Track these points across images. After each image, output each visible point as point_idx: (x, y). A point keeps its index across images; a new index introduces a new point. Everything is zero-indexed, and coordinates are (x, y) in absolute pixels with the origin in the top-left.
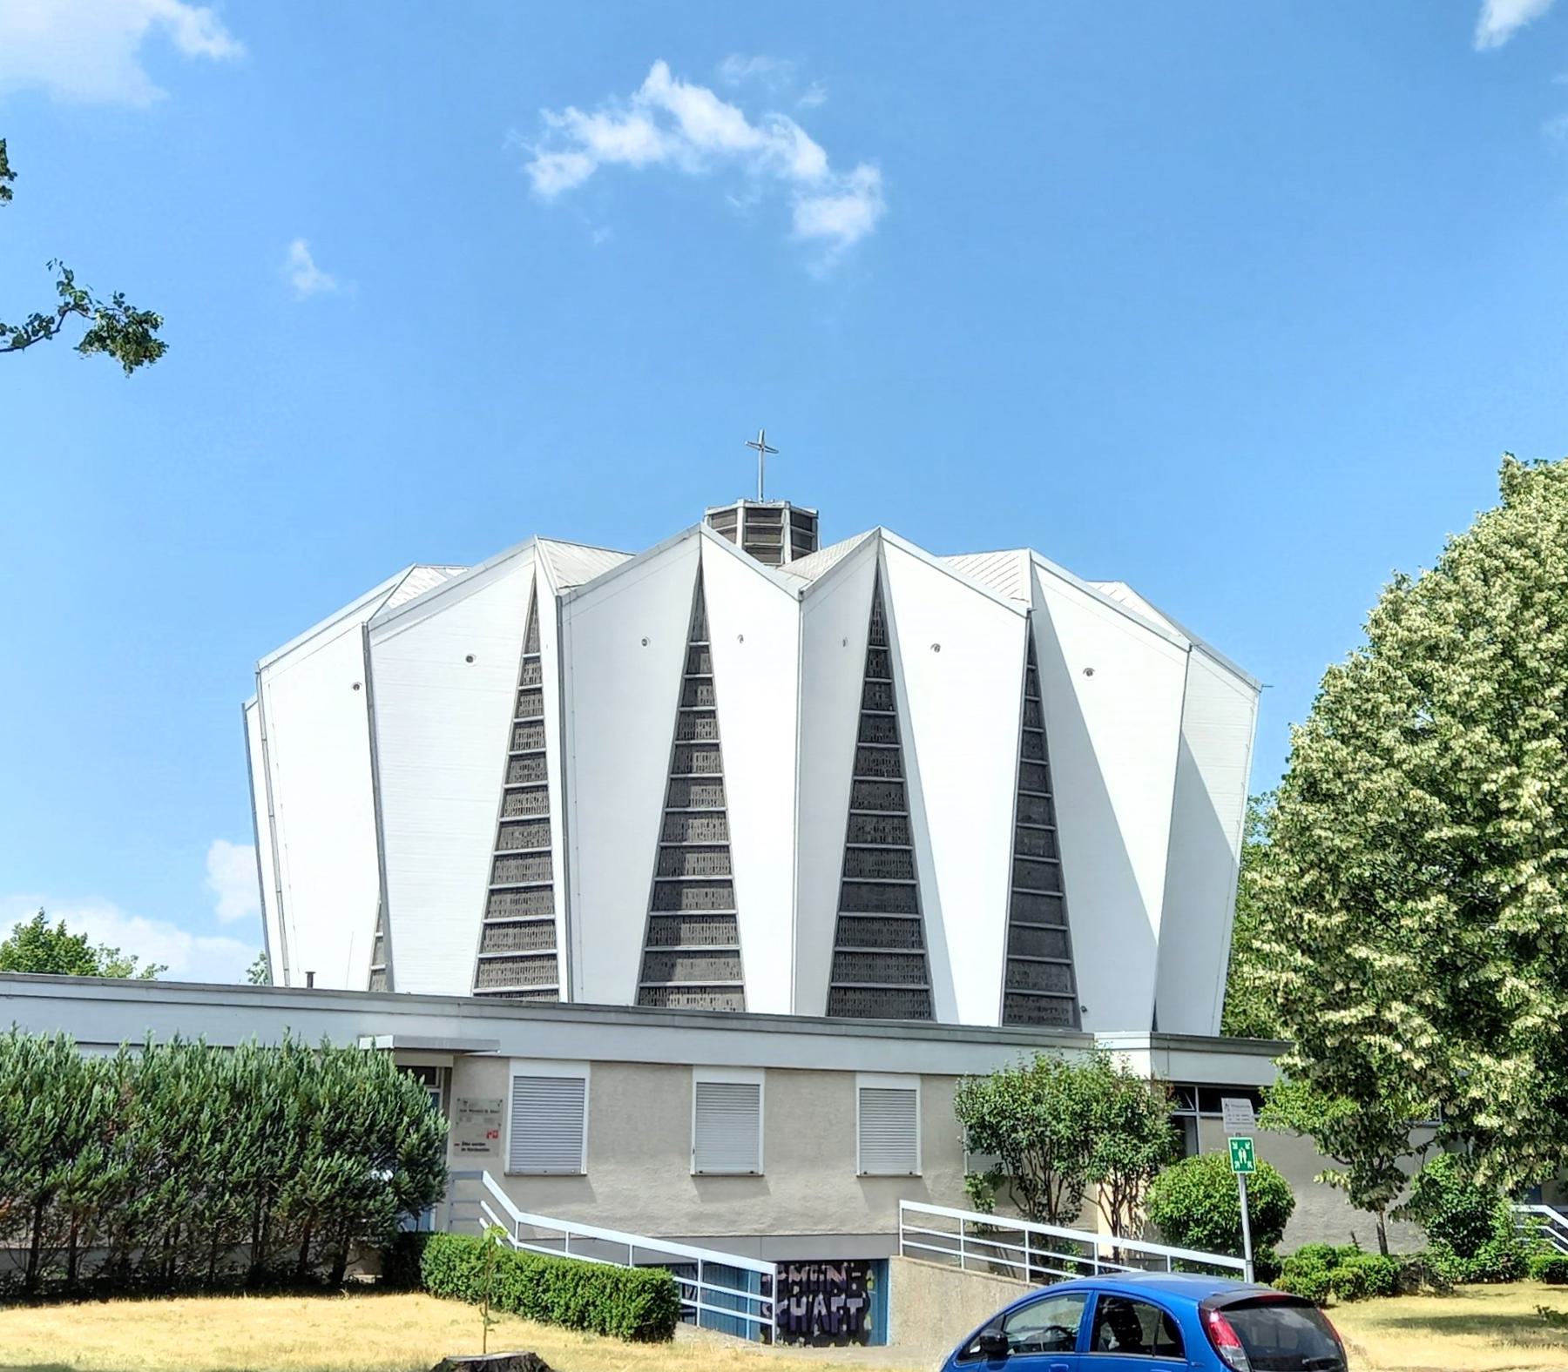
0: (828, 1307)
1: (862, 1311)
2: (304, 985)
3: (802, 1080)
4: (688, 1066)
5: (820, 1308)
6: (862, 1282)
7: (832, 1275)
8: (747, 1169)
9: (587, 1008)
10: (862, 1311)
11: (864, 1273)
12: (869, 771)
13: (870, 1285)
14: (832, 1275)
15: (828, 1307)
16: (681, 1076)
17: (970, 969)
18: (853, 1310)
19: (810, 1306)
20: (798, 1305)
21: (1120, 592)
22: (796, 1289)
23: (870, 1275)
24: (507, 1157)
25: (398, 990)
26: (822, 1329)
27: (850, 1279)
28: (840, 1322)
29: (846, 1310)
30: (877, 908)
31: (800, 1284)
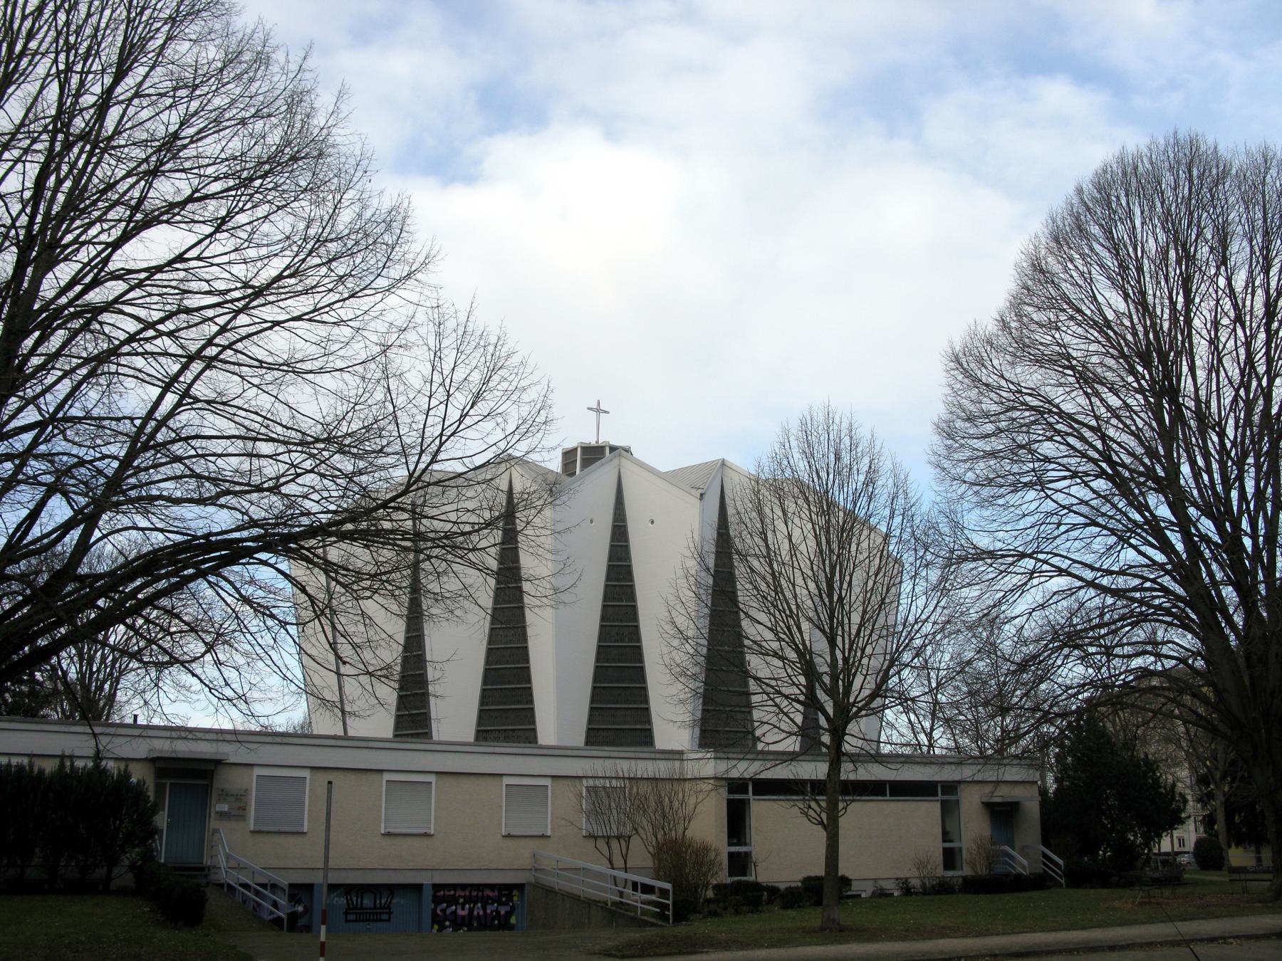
0: (485, 911)
1: (509, 914)
2: (342, 734)
3: (464, 780)
4: (381, 771)
5: (478, 910)
6: (510, 898)
7: (488, 893)
8: (422, 831)
9: (353, 739)
10: (509, 914)
11: (511, 891)
12: (614, 599)
13: (515, 898)
14: (488, 893)
15: (485, 911)
16: (375, 776)
17: (673, 713)
18: (503, 912)
19: (471, 910)
20: (463, 909)
21: (10, 91)
22: (461, 900)
23: (515, 892)
24: (252, 822)
25: (351, 733)
26: (479, 923)
27: (501, 895)
28: (493, 919)
29: (498, 912)
30: (618, 682)
31: (464, 897)
